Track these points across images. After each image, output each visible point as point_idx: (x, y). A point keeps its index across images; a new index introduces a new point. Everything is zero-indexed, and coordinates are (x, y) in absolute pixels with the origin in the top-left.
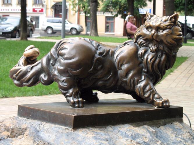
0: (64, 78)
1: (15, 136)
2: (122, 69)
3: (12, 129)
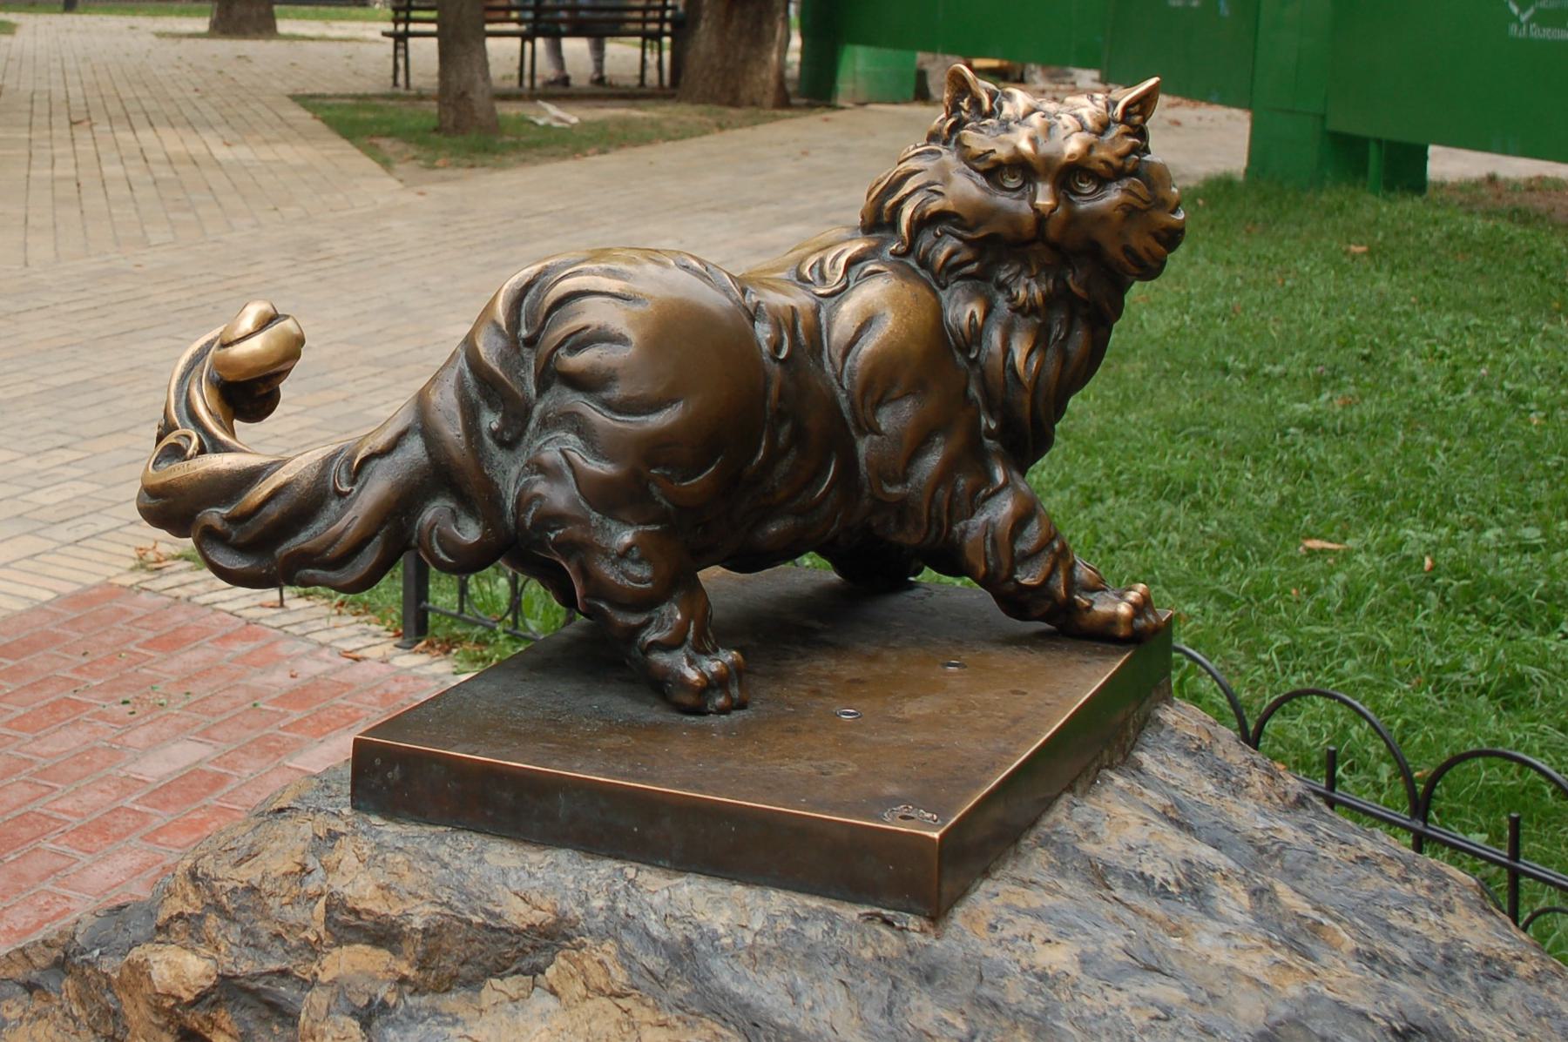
0: (626, 537)
1: (457, 976)
2: (883, 428)
3: (425, 930)
